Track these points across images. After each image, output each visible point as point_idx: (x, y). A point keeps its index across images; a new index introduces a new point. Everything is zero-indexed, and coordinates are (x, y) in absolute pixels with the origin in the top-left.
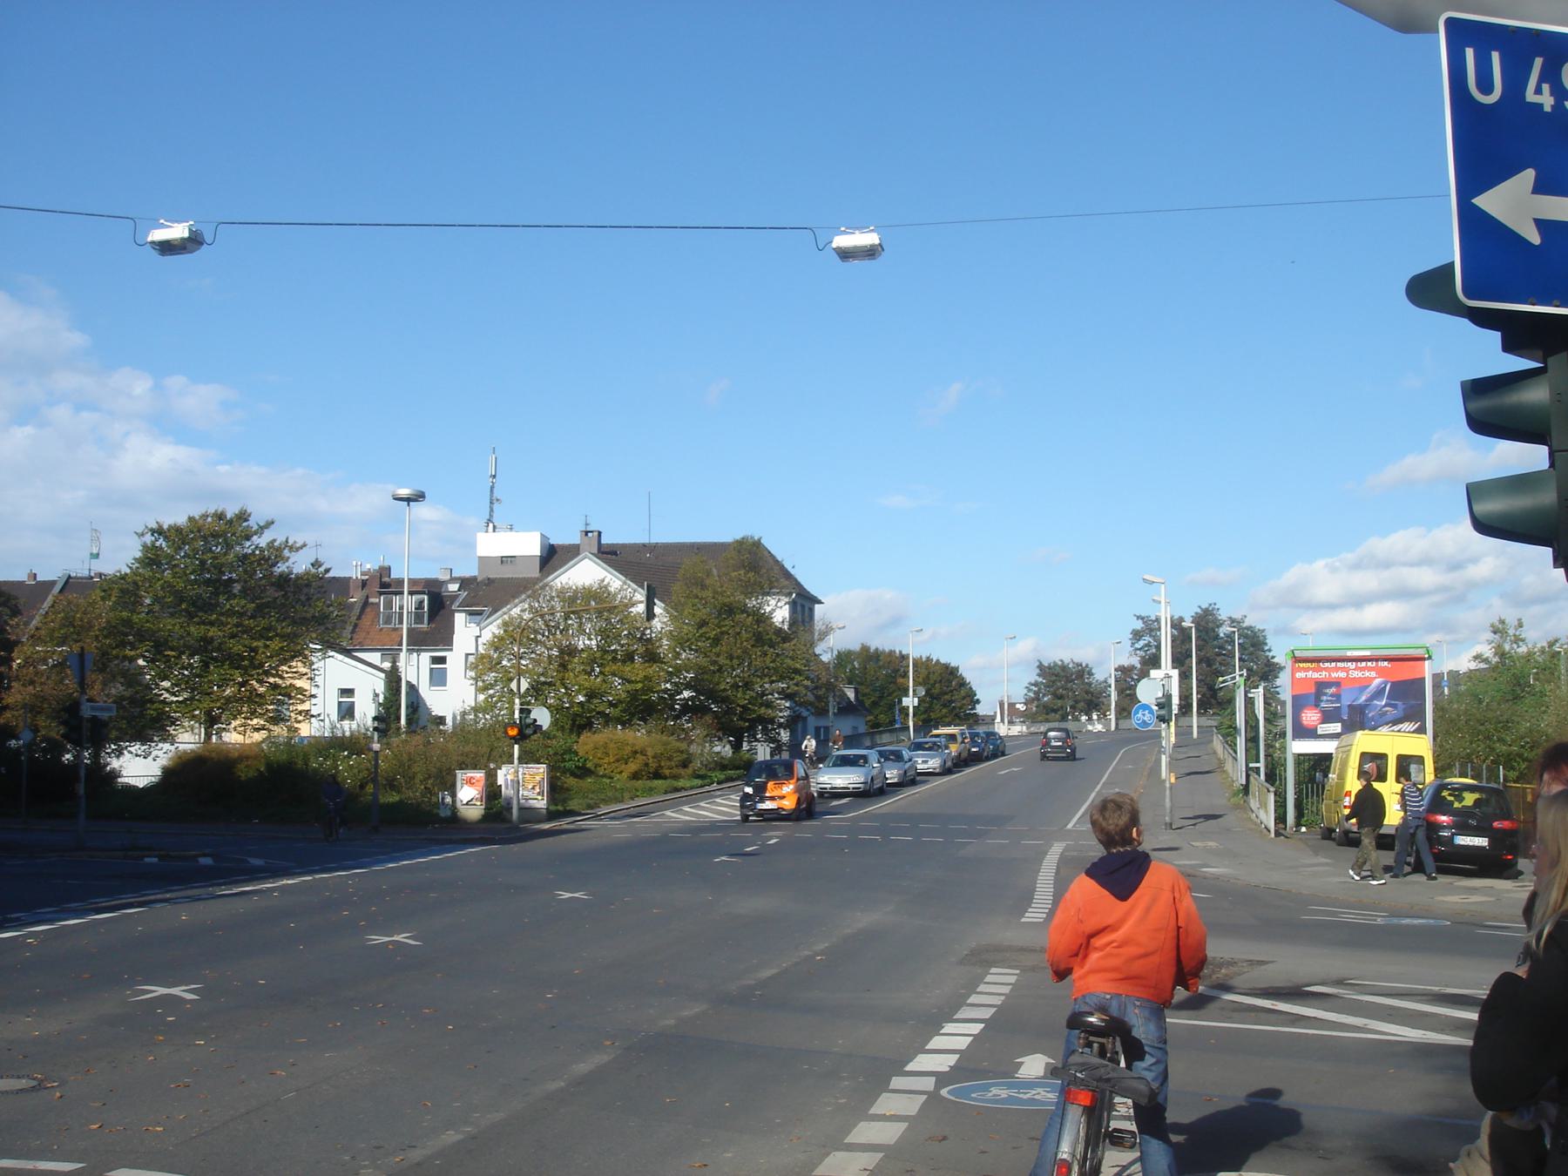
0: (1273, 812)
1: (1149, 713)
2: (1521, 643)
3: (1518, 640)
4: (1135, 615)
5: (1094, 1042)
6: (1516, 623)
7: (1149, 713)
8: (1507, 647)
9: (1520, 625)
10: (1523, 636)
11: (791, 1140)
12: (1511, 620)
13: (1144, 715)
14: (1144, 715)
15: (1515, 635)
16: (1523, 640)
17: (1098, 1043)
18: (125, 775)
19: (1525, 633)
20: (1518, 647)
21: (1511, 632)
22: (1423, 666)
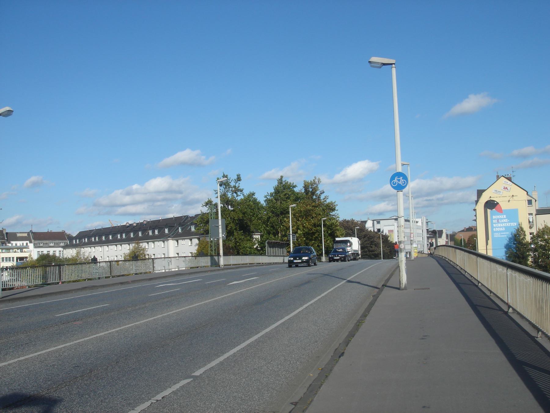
0: (541, 272)
1: (403, 179)
2: (239, 193)
3: (237, 190)
4: (223, 173)
5: (531, 266)
6: (236, 177)
7: (403, 179)
8: (229, 195)
9: (239, 179)
10: (241, 188)
11: (417, 222)
12: (232, 177)
13: (399, 180)
14: (399, 180)
15: (235, 187)
16: (241, 191)
17: (527, 265)
18: (508, 270)
19: (241, 185)
20: (237, 196)
21: (232, 184)
22: (224, 263)
